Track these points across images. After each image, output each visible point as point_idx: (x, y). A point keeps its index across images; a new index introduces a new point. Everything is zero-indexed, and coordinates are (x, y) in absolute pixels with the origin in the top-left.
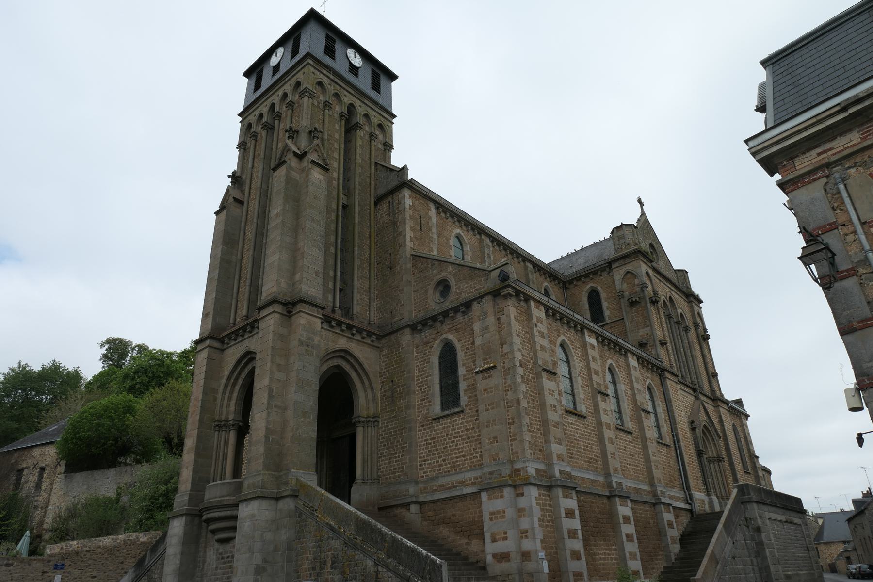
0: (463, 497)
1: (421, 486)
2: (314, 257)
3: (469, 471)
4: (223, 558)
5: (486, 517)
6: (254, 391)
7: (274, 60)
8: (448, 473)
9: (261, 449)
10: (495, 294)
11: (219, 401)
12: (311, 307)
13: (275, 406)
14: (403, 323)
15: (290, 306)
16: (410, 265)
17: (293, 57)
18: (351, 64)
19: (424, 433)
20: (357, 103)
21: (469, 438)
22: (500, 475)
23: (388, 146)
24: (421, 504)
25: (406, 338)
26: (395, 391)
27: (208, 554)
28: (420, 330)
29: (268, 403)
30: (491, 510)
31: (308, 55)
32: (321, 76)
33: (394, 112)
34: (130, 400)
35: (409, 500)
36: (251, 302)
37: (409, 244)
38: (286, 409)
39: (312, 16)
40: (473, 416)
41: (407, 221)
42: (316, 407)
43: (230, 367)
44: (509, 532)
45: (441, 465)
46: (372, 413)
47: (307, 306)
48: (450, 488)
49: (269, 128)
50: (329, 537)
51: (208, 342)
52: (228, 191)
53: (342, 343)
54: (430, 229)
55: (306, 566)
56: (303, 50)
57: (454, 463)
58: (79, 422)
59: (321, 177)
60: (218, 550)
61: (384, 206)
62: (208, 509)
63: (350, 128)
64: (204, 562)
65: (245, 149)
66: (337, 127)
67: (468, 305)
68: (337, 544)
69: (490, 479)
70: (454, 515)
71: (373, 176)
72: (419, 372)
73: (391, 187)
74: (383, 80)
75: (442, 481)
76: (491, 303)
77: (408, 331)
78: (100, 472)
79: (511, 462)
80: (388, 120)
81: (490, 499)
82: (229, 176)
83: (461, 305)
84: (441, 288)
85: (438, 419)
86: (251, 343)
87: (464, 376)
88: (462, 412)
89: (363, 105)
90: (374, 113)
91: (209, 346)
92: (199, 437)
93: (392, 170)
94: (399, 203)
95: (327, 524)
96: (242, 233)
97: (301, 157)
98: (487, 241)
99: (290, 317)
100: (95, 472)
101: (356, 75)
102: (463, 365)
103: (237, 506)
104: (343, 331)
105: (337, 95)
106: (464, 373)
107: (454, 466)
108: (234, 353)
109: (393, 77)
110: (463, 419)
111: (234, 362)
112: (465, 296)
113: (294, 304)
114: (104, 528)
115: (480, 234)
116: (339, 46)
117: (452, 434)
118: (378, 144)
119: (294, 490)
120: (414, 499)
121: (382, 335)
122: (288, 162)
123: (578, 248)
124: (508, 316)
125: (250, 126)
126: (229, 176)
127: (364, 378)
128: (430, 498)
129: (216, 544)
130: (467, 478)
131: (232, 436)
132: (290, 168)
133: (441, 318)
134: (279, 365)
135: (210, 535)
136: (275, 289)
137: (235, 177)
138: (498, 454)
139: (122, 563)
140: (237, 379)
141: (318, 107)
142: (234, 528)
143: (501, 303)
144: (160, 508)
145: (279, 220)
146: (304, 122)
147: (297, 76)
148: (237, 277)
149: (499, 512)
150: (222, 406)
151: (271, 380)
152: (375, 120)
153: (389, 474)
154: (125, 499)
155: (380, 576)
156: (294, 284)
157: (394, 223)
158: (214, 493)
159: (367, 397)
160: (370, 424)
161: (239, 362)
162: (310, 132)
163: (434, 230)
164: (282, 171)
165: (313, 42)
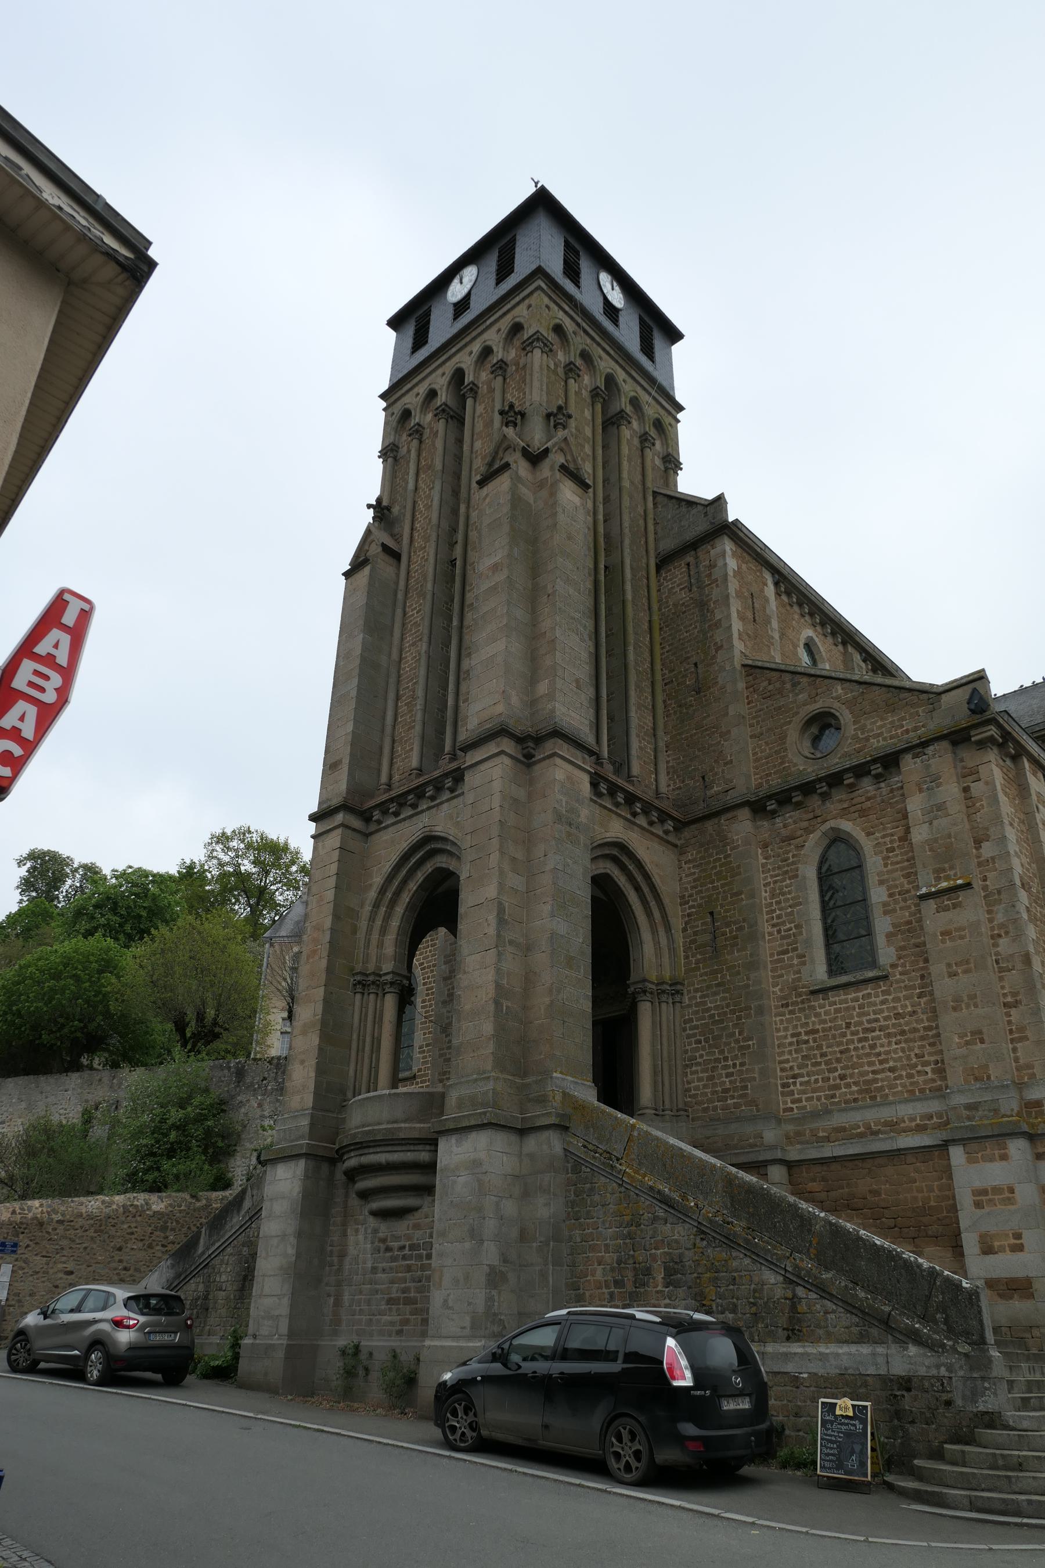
0: (897, 1155)
1: (790, 1128)
2: (572, 650)
3: (906, 1101)
4: (388, 1249)
5: (965, 1200)
6: (462, 910)
7: (456, 291)
8: (852, 1104)
9: (488, 1028)
10: (958, 738)
11: (361, 935)
12: (573, 750)
13: (511, 942)
14: (731, 798)
15: (530, 743)
16: (741, 685)
17: (499, 280)
18: (607, 302)
19: (789, 1021)
20: (621, 375)
21: (903, 1033)
22: (996, 1111)
23: (672, 464)
24: (790, 1165)
25: (742, 827)
26: (719, 933)
27: (351, 1239)
28: (774, 812)
29: (499, 936)
30: (978, 1184)
31: (539, 272)
32: (561, 314)
33: (680, 397)
34: (109, 949)
35: (768, 1156)
36: (433, 743)
37: (738, 646)
38: (516, 953)
39: (542, 204)
40: (913, 987)
41: (732, 600)
42: (589, 951)
43: (387, 867)
44: (1026, 1234)
45: (837, 1087)
46: (667, 974)
47: (565, 746)
48: (861, 1135)
49: (455, 417)
50: (655, 1219)
51: (340, 817)
52: (368, 532)
53: (616, 830)
54: (767, 621)
55: (599, 1275)
56: (523, 266)
57: (866, 1082)
58: (19, 983)
59: (577, 500)
60: (375, 1231)
61: (677, 573)
62: (361, 1146)
63: (612, 422)
64: (342, 1255)
65: (395, 459)
66: (587, 414)
67: (890, 761)
68: (680, 1232)
69: (969, 1118)
70: (876, 1193)
71: (651, 516)
72: (773, 896)
73: (689, 536)
74: (658, 342)
75: (839, 1120)
76: (949, 757)
77: (745, 813)
78: (52, 1079)
79: (1020, 1086)
80: (670, 413)
81: (971, 1160)
82: (369, 506)
83: (874, 761)
84: (814, 730)
85: (822, 991)
86: (439, 819)
87: (885, 904)
88: (885, 977)
89: (629, 380)
90: (650, 400)
91: (342, 825)
92: (327, 1002)
93: (690, 503)
94: (712, 566)
95: (651, 1188)
96: (399, 611)
97: (535, 459)
98: (857, 657)
99: (529, 766)
100: (42, 1078)
101: (615, 322)
102: (881, 882)
103: (432, 1143)
104: (617, 805)
105: (585, 356)
106: (885, 898)
107: (867, 1091)
108: (394, 841)
109: (674, 335)
110: (884, 993)
111: (394, 857)
112: (880, 744)
113: (539, 740)
114: (78, 1179)
115: (844, 643)
116: (586, 266)
117: (860, 1023)
118: (654, 458)
119: (562, 1116)
120: (779, 1155)
121: (687, 820)
122: (513, 466)
123: (1028, 683)
124: (990, 783)
125: (406, 414)
126: (369, 506)
127: (653, 904)
128: (813, 1154)
129: (371, 1219)
130: (905, 1118)
131: (390, 1002)
132: (517, 479)
133: (771, 806)
134: (514, 859)
135: (354, 1201)
136: (500, 708)
137: (381, 510)
138: (986, 1067)
139: (120, 1249)
140: (398, 893)
141: (555, 372)
142: (429, 1190)
143: (970, 757)
144: (171, 1153)
145: (501, 576)
146: (536, 395)
147: (516, 312)
148: (391, 695)
149: (997, 1190)
150: (367, 945)
151: (501, 886)
152: (651, 411)
153: (710, 1101)
154: (99, 1132)
155: (803, 1307)
156: (533, 703)
157: (702, 605)
158: (371, 1112)
159: (657, 943)
160: (664, 998)
161: (405, 857)
162: (548, 416)
163: (775, 624)
164: (502, 484)
165: (542, 249)
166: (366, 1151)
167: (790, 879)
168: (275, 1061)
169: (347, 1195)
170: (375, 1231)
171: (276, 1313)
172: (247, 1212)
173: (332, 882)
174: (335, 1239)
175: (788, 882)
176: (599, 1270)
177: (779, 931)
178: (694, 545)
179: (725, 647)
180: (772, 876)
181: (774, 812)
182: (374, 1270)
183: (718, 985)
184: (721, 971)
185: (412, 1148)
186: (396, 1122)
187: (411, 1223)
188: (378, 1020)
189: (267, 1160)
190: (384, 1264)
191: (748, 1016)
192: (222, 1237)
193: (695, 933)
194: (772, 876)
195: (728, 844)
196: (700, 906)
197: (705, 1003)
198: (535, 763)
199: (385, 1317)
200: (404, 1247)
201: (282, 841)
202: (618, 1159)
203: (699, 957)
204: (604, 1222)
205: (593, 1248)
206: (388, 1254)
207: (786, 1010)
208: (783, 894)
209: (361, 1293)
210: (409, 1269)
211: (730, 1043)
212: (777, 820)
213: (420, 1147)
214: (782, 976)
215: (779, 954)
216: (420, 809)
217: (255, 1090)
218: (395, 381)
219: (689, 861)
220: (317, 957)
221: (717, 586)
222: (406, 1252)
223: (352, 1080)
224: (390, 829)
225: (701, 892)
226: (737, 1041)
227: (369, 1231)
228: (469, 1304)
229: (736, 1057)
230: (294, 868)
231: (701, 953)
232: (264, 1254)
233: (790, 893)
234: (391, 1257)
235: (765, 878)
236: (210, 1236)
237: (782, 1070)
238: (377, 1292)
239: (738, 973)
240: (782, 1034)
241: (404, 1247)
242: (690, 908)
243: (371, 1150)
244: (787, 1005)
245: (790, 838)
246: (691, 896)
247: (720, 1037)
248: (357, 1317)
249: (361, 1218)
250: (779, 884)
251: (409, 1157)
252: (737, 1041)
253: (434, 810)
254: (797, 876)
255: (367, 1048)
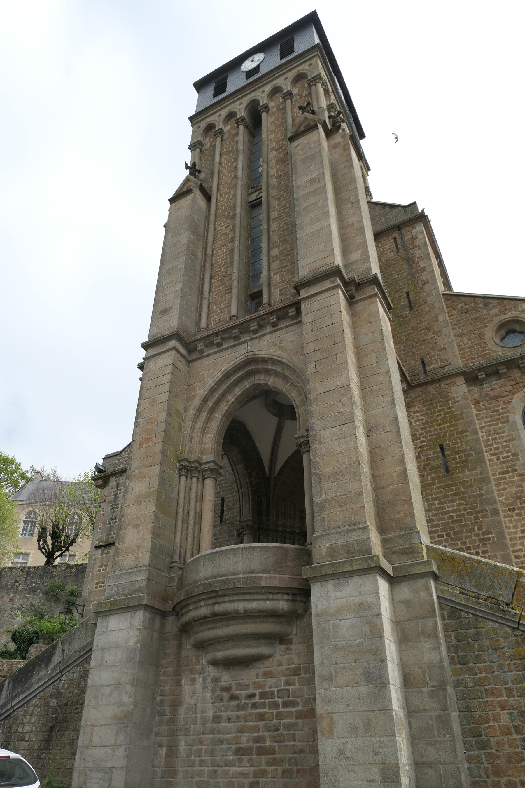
4: (233, 698)
7: (248, 65)
27: (186, 688)
43: (211, 382)
51: (173, 343)
62: (214, 594)
72: (489, 435)
77: (461, 381)
84: (503, 332)
92: (161, 477)
135: (188, 650)
140: (217, 404)
157: (409, 260)
161: (227, 376)
166: (221, 599)
167: (502, 423)
168: (26, 570)
169: (180, 646)
170: (216, 680)
171: (109, 765)
172: (56, 666)
173: (166, 388)
174: (167, 688)
175: (501, 425)
176: (504, 715)
177: (498, 459)
178: (399, 227)
179: (430, 282)
180: (486, 422)
181: (483, 380)
182: (217, 719)
183: (455, 495)
184: (456, 485)
185: (271, 596)
186: (253, 572)
187: (261, 671)
188: (201, 499)
189: (106, 611)
190: (229, 713)
191: (485, 516)
192: (28, 689)
193: (428, 459)
194: (486, 422)
195: (450, 400)
196: (430, 440)
197: (444, 508)
198: (357, 302)
199: (234, 769)
200: (253, 695)
201: (10, 457)
202: (507, 604)
203: (433, 475)
204: (500, 666)
205: (490, 693)
206: (234, 703)
207: (514, 513)
208: (498, 433)
209: (201, 742)
210: (261, 717)
211: (471, 537)
212: (485, 386)
213: (279, 596)
214: (506, 489)
215: (500, 474)
216: (242, 340)
217: (8, 589)
218: (198, 111)
219: (417, 412)
220: (150, 443)
221: (419, 249)
222: (257, 699)
223: (179, 545)
224: (212, 357)
225: (430, 431)
226: (477, 535)
227: (209, 680)
228: (376, 754)
229: (478, 547)
230: (16, 474)
231: (434, 473)
232: (93, 703)
233: (503, 432)
234: (238, 706)
235: (481, 423)
236: (13, 688)
237: (517, 557)
238: (221, 741)
239: (471, 486)
240: (512, 530)
241: (253, 695)
242: (421, 442)
243: (227, 599)
244: (514, 509)
245: (497, 398)
246: (421, 434)
247: (461, 532)
248: (197, 768)
249: (198, 667)
250: (493, 427)
251: (268, 605)
252: (477, 535)
253: (256, 341)
254: (508, 421)
255: (191, 520)
